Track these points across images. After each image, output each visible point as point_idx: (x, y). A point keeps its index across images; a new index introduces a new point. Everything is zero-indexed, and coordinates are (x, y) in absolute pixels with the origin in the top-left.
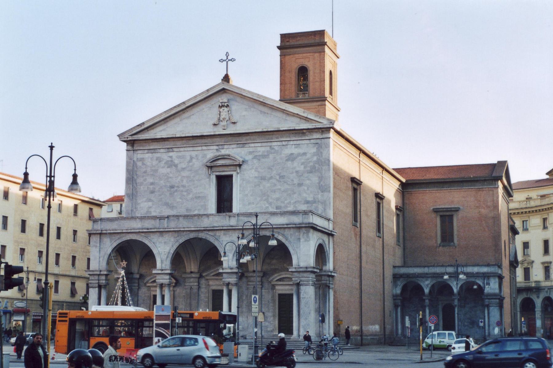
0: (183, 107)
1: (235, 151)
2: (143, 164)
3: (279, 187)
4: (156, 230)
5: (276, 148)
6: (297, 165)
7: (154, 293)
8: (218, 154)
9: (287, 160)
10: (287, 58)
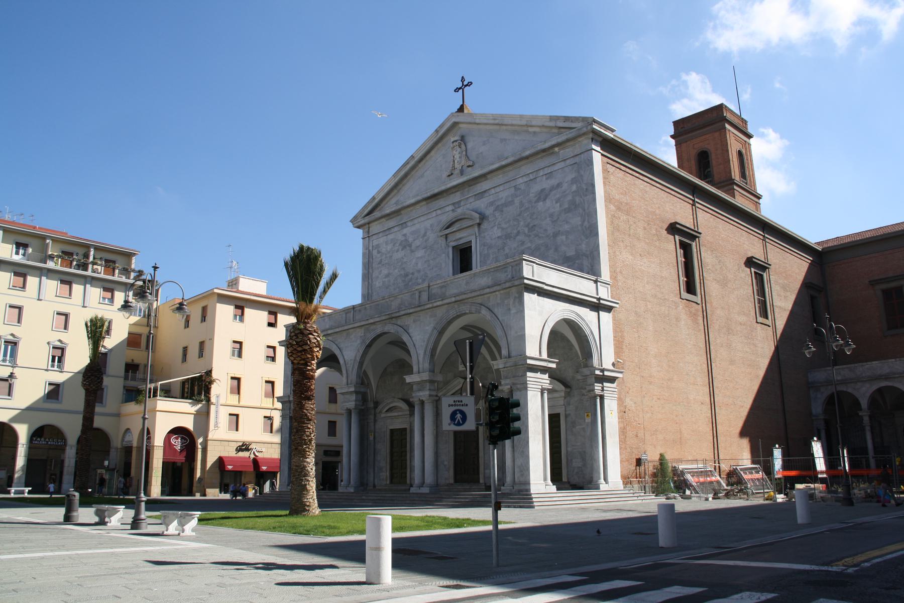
0: (412, 163)
1: (470, 205)
2: (379, 252)
3: (529, 245)
4: (340, 329)
5: (523, 187)
6: (550, 205)
7: (397, 425)
8: (455, 214)
9: (537, 201)
10: (684, 145)
